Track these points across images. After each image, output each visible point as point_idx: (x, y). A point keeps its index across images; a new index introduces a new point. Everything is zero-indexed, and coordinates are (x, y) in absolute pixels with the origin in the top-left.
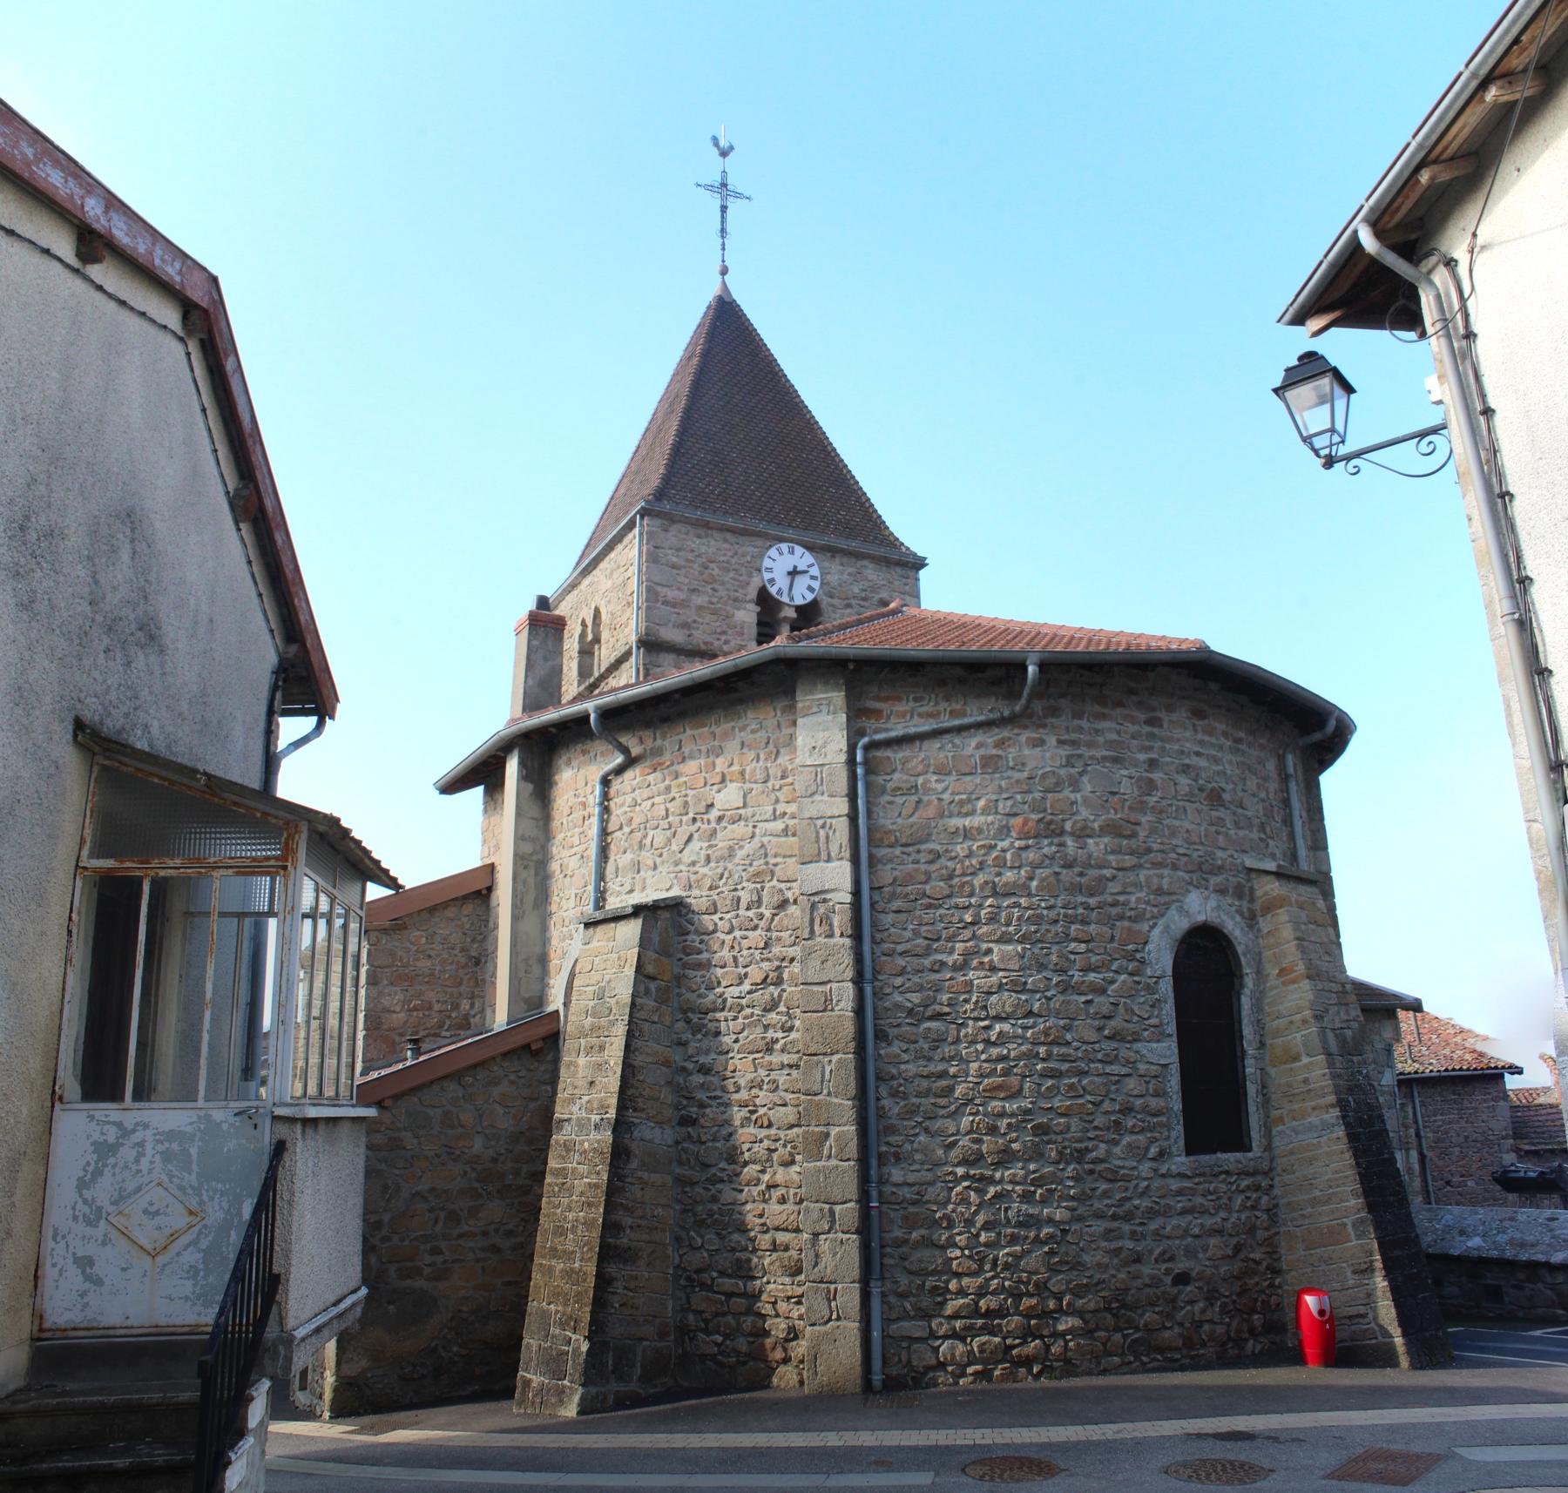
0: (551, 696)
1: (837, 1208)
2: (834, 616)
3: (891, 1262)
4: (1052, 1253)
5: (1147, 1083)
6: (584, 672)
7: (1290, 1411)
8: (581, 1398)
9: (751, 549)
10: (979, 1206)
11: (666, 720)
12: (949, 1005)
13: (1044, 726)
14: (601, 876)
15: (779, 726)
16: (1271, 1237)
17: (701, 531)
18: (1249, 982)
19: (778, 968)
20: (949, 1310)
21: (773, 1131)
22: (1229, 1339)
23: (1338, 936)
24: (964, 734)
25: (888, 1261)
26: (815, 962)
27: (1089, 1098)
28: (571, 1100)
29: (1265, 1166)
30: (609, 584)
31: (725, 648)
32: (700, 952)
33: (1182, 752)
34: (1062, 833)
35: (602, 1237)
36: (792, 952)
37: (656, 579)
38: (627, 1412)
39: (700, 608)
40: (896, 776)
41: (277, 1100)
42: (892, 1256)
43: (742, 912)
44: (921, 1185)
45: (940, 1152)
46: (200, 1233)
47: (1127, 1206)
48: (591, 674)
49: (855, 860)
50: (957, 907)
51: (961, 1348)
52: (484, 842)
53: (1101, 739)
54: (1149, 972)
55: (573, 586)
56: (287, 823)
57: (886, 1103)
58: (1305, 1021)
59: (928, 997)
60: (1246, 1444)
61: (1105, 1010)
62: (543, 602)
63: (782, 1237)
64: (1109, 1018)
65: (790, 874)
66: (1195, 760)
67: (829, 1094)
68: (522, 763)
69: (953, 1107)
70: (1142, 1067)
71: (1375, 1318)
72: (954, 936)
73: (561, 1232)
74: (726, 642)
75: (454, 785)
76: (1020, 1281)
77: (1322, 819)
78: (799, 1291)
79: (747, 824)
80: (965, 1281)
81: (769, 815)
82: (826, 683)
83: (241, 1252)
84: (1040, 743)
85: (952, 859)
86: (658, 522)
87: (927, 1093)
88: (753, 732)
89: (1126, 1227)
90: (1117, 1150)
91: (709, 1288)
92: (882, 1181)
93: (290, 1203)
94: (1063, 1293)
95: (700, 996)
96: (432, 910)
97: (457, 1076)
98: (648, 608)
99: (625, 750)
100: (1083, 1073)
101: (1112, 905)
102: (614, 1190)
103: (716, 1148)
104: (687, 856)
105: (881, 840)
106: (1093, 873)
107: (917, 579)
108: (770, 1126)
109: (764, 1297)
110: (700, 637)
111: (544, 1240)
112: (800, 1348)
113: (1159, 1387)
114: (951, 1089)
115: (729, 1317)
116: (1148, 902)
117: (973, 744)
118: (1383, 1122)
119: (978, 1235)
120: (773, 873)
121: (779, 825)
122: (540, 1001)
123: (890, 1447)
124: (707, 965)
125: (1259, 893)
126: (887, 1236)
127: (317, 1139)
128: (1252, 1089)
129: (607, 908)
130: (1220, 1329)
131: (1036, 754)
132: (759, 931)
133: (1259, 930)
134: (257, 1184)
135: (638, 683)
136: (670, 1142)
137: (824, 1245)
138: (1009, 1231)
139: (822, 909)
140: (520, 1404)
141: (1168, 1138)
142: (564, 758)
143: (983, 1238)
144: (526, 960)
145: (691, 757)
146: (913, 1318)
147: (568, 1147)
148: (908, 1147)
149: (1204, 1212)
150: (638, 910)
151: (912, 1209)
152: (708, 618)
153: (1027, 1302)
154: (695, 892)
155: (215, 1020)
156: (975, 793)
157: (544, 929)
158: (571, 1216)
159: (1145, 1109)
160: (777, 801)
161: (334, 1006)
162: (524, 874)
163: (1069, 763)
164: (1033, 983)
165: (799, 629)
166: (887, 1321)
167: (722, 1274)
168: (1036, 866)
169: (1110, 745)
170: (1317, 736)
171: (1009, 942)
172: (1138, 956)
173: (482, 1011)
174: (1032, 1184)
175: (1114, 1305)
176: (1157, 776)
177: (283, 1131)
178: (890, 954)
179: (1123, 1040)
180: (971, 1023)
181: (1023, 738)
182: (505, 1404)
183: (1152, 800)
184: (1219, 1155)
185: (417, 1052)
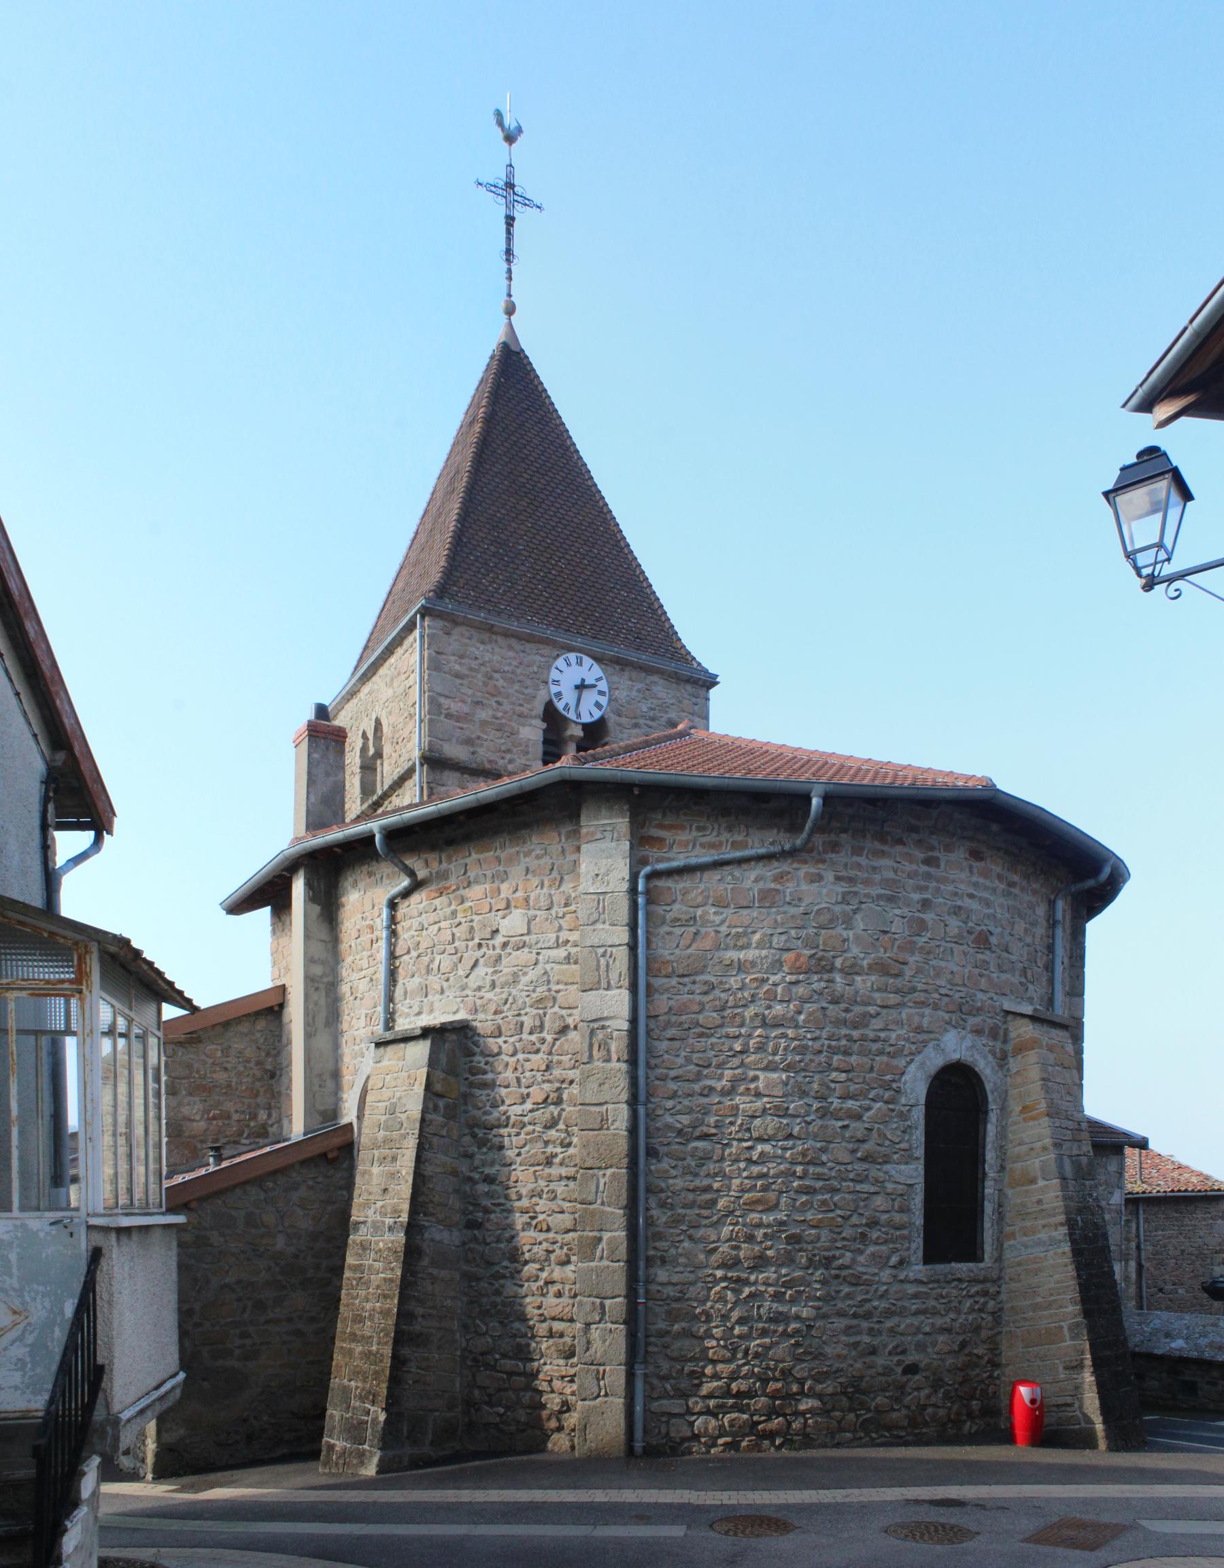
0: (335, 814)
1: (608, 1302)
2: (620, 737)
3: (656, 1349)
4: (797, 1345)
5: (893, 1200)
6: (367, 789)
7: (997, 1483)
8: (380, 1460)
9: (538, 658)
10: (735, 1303)
11: (451, 843)
12: (716, 1127)
13: (824, 861)
14: (390, 998)
15: (563, 851)
16: (993, 1336)
17: (486, 636)
18: (993, 1117)
19: (558, 1089)
20: (705, 1390)
21: (551, 1235)
22: (950, 1420)
23: (1081, 1078)
24: (745, 866)
25: (651, 1349)
26: (593, 1085)
27: (839, 1212)
28: (367, 1205)
29: (994, 1275)
30: (390, 692)
31: (510, 767)
32: (485, 1073)
33: (956, 894)
34: (831, 969)
35: (397, 1325)
36: (571, 1074)
37: (439, 689)
38: (420, 1471)
39: (484, 723)
40: (676, 907)
41: (90, 1210)
42: (656, 1345)
43: (525, 1036)
44: (684, 1284)
45: (702, 1257)
46: (25, 1330)
47: (867, 1306)
48: (374, 792)
49: (633, 988)
50: (727, 1036)
51: (713, 1423)
52: (274, 964)
53: (877, 877)
54: (903, 1100)
55: (352, 694)
56: (76, 943)
57: (655, 1212)
58: (1044, 1148)
59: (697, 1119)
60: (955, 1510)
61: (859, 1135)
62: (322, 711)
63: (558, 1326)
64: (863, 1141)
65: (571, 1001)
66: (967, 903)
67: (603, 1204)
68: (309, 885)
69: (715, 1218)
70: (890, 1186)
71: (1081, 1407)
72: (724, 1063)
73: (358, 1319)
74: (511, 761)
75: (242, 904)
76: (768, 1368)
77: (1083, 966)
78: (572, 1371)
79: (529, 950)
80: (720, 1367)
81: (552, 942)
82: (611, 808)
83: (66, 1348)
84: (819, 878)
85: (724, 991)
86: (440, 623)
87: (691, 1205)
88: (538, 857)
89: (865, 1325)
90: (861, 1259)
91: (493, 1368)
92: (648, 1281)
93: (110, 1303)
94: (805, 1379)
95: (485, 1113)
96: (226, 1025)
97: (258, 1181)
98: (430, 721)
99: (411, 873)
100: (835, 1191)
101: (873, 1041)
102: (407, 1285)
103: (500, 1249)
104: (473, 981)
105: (659, 970)
106: (858, 1009)
107: (707, 699)
108: (548, 1230)
109: (541, 1376)
110: (485, 755)
111: (343, 1327)
112: (572, 1419)
113: (884, 1460)
114: (714, 1202)
115: (510, 1393)
116: (907, 1040)
117: (752, 878)
118: (1107, 1239)
119: (732, 1328)
120: (554, 999)
121: (561, 953)
122: (334, 1113)
123: (648, 1504)
124: (491, 1085)
125: (1012, 1035)
126: (653, 1327)
127: (133, 1244)
128: (988, 1208)
129: (397, 1029)
130: (942, 1412)
131: (813, 888)
132: (541, 1055)
133: (1008, 1070)
134: (77, 1287)
135: (421, 803)
136: (457, 1243)
137: (595, 1333)
138: (760, 1325)
139: (600, 1035)
140: (325, 1465)
141: (908, 1249)
142: (350, 880)
143: (737, 1331)
144: (320, 1075)
145: (477, 882)
146: (672, 1397)
147: (365, 1247)
148: (673, 1251)
149: (935, 1313)
150: (426, 1032)
151: (675, 1305)
152: (494, 734)
153: (773, 1386)
154: (481, 1016)
155: (21, 1133)
156: (753, 924)
157: (336, 1046)
158: (368, 1306)
159: (889, 1224)
160: (560, 929)
161: (139, 1113)
162: (315, 996)
163: (844, 901)
164: (795, 1108)
165: (586, 750)
166: (649, 1398)
167: (504, 1356)
168: (804, 1001)
169: (886, 883)
170: (1090, 883)
171: (774, 1070)
172: (894, 1085)
173: (279, 1121)
174: (783, 1286)
175: (850, 1390)
176: (929, 917)
177: (98, 1239)
178: (663, 1079)
179: (874, 1162)
180: (735, 1143)
181: (801, 873)
182: (314, 1463)
183: (921, 941)
184: (953, 1264)
185: (219, 1159)
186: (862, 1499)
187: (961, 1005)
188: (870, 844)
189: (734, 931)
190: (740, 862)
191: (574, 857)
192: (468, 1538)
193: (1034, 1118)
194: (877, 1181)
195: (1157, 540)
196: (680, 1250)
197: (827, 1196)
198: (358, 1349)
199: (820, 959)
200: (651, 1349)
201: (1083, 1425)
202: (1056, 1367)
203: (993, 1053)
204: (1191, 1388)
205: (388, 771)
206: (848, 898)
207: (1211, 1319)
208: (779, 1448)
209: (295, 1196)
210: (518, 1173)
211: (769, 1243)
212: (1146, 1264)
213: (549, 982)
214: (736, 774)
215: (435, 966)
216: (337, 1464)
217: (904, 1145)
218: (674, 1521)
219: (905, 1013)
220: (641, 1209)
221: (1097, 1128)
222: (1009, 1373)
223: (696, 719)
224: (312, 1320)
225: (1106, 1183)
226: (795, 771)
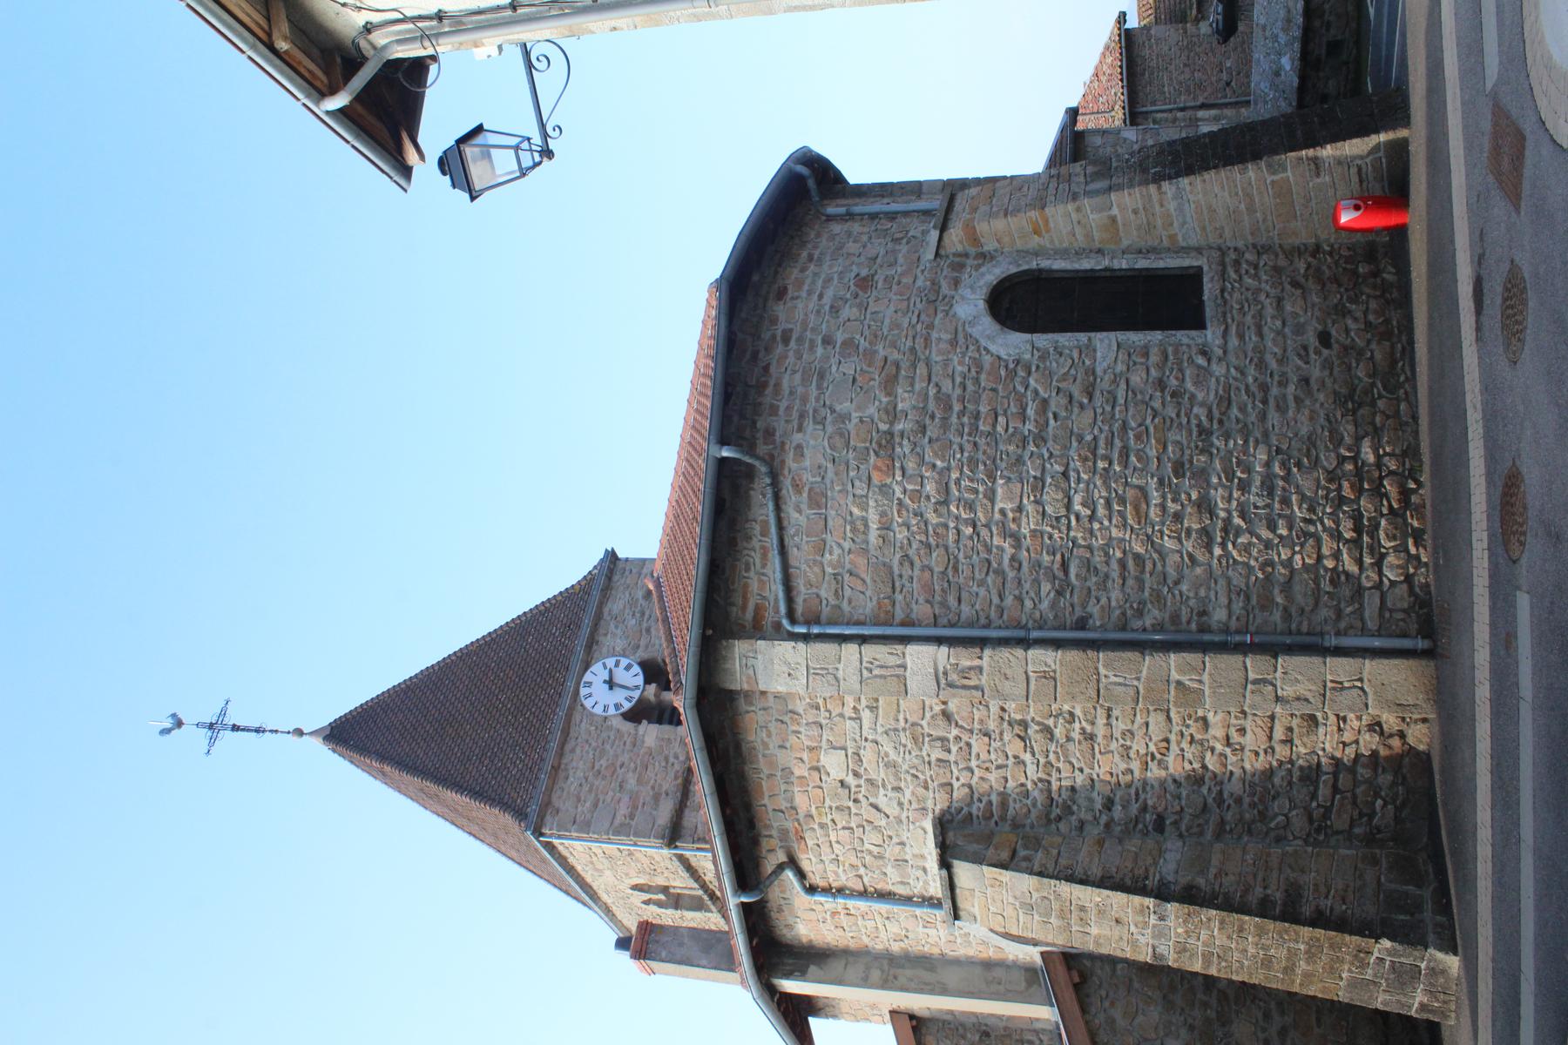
0: (719, 941)
1: (1252, 676)
2: (658, 648)
3: (1305, 623)
4: (1299, 465)
6: (698, 906)
7: (1452, 242)
10: (1252, 533)
11: (751, 823)
13: (783, 443)
14: (907, 900)
17: (562, 774)
18: (1045, 264)
19: (1010, 724)
20: (1353, 568)
21: (1173, 737)
23: (1005, 178)
24: (785, 523)
25: (1305, 628)
27: (1148, 421)
28: (1134, 943)
30: (608, 873)
31: (682, 758)
32: (990, 803)
33: (818, 312)
35: (1274, 919)
36: (994, 709)
37: (607, 825)
38: (1454, 903)
39: (639, 781)
40: (823, 594)
42: (1300, 623)
43: (952, 758)
45: (1199, 570)
47: (1254, 388)
48: (700, 898)
49: (905, 640)
50: (957, 541)
51: (1391, 559)
53: (800, 390)
54: (1027, 356)
57: (1148, 622)
58: (1078, 210)
60: (1486, 286)
61: (1064, 401)
62: (622, 944)
63: (1279, 733)
64: (1071, 397)
66: (827, 300)
67: (1138, 679)
69: (1155, 556)
70: (1120, 367)
71: (1362, 158)
72: (986, 545)
73: (1267, 962)
74: (676, 757)
76: (1326, 497)
77: (892, 184)
78: (1332, 718)
79: (865, 746)
80: (1325, 551)
82: (724, 658)
84: (799, 447)
86: (548, 818)
88: (769, 735)
89: (1275, 391)
90: (1200, 396)
91: (1328, 810)
94: (1338, 455)
95: (1034, 805)
98: (636, 835)
99: (781, 868)
101: (965, 389)
104: (893, 810)
105: (887, 612)
106: (932, 406)
108: (1167, 740)
109: (1338, 754)
110: (670, 783)
111: (1275, 980)
112: (1390, 721)
113: (1430, 367)
114: (1137, 556)
115: (1358, 791)
116: (964, 354)
119: (1281, 537)
121: (866, 715)
122: (1030, 971)
124: (1004, 797)
125: (960, 248)
128: (1142, 263)
129: (940, 895)
131: (809, 454)
132: (973, 742)
135: (712, 850)
137: (1287, 691)
138: (1277, 506)
139: (953, 677)
142: (785, 931)
143: (1284, 532)
145: (792, 800)
146: (1362, 605)
147: (1182, 949)
148: (1192, 602)
150: (945, 864)
151: (1254, 601)
152: (650, 773)
153: (1347, 491)
154: (930, 804)
156: (844, 517)
157: (957, 962)
158: (1251, 950)
159: (1161, 366)
160: (841, 715)
162: (902, 980)
165: (669, 682)
166: (1364, 631)
167: (1314, 796)
169: (806, 380)
170: (811, 183)
171: (993, 492)
172: (1011, 366)
173: (1036, 1032)
176: (840, 337)
178: (1001, 610)
179: (1093, 385)
180: (1072, 534)
181: (794, 466)
183: (863, 344)
184: (1205, 298)
186: (1477, 390)
187: (929, 302)
188: (767, 399)
189: (849, 534)
190: (781, 528)
191: (771, 699)
192: (1537, 851)
193: (1046, 222)
194: (1114, 381)
195: (512, 152)
196: (1191, 595)
197: (1131, 434)
198: (1303, 965)
199: (880, 445)
200: (1305, 628)
201: (1381, 154)
202: (1319, 188)
203: (978, 267)
204: (1334, 47)
205: (681, 882)
206: (819, 418)
207: (1257, 32)
208: (1419, 484)
209: (1121, 1022)
210: (1101, 772)
211: (1183, 496)
212: (1201, 100)
213: (896, 730)
214: (697, 531)
215: (875, 850)
216: (1445, 1002)
217: (1075, 355)
218: (1513, 605)
219: (936, 357)
220: (1144, 637)
221: (1055, 159)
222: (1326, 235)
223: (645, 571)
224: (1267, 1016)
225: (1114, 146)
226: (696, 474)
